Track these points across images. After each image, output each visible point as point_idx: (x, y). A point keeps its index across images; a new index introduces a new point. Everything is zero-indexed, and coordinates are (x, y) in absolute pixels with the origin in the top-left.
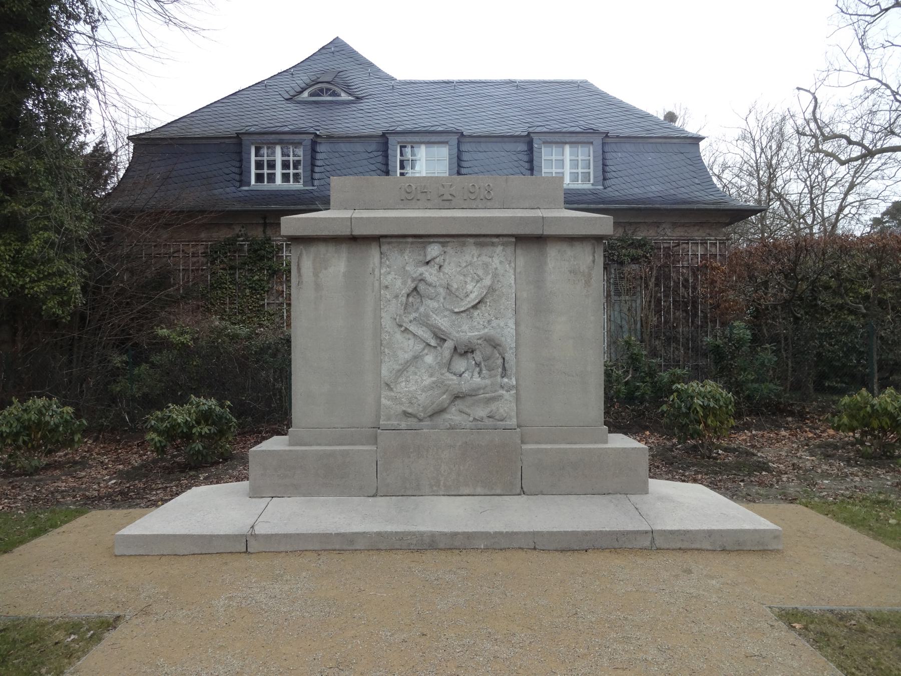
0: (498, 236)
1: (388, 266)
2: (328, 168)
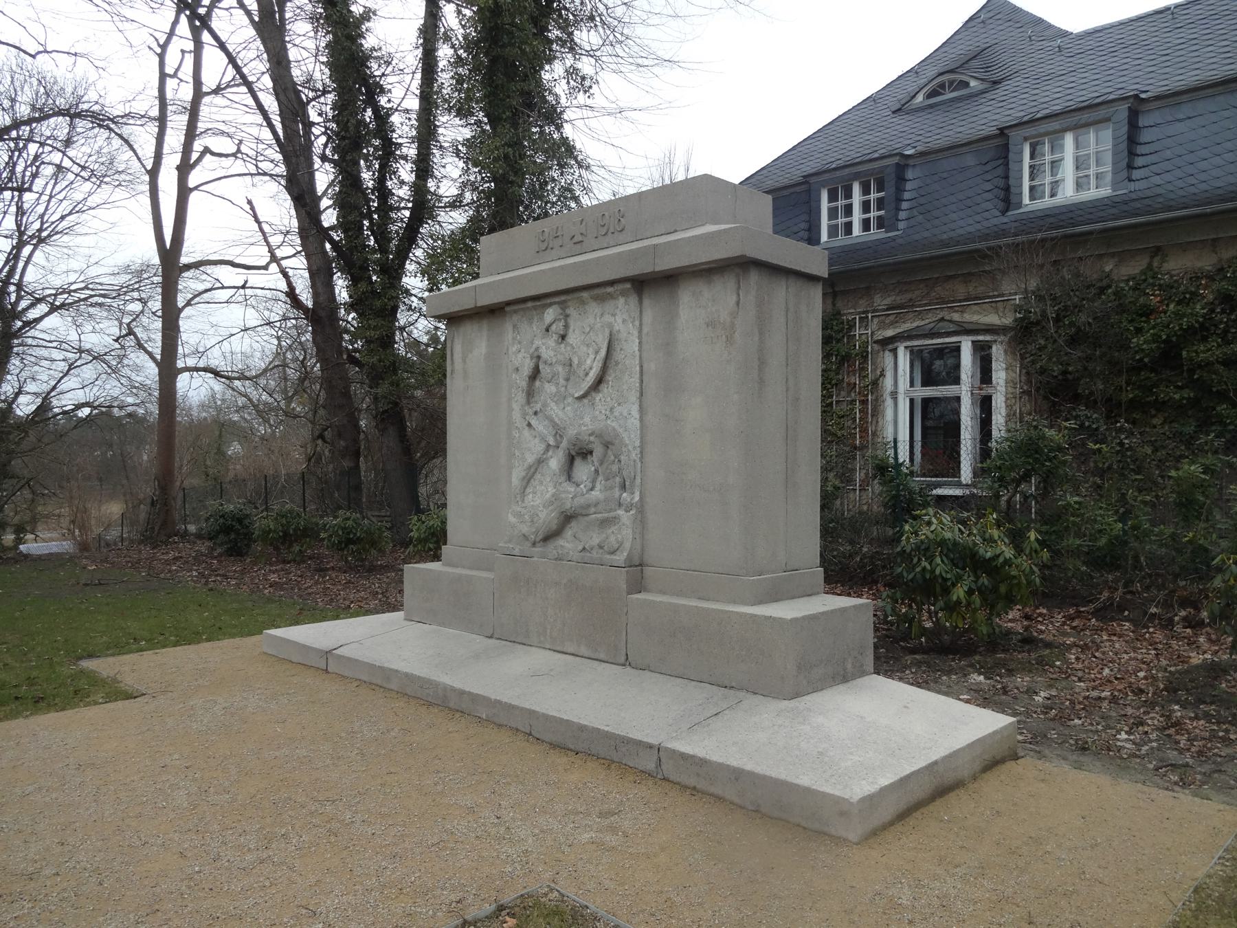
0: (612, 283)
1: (520, 343)
2: (922, 200)
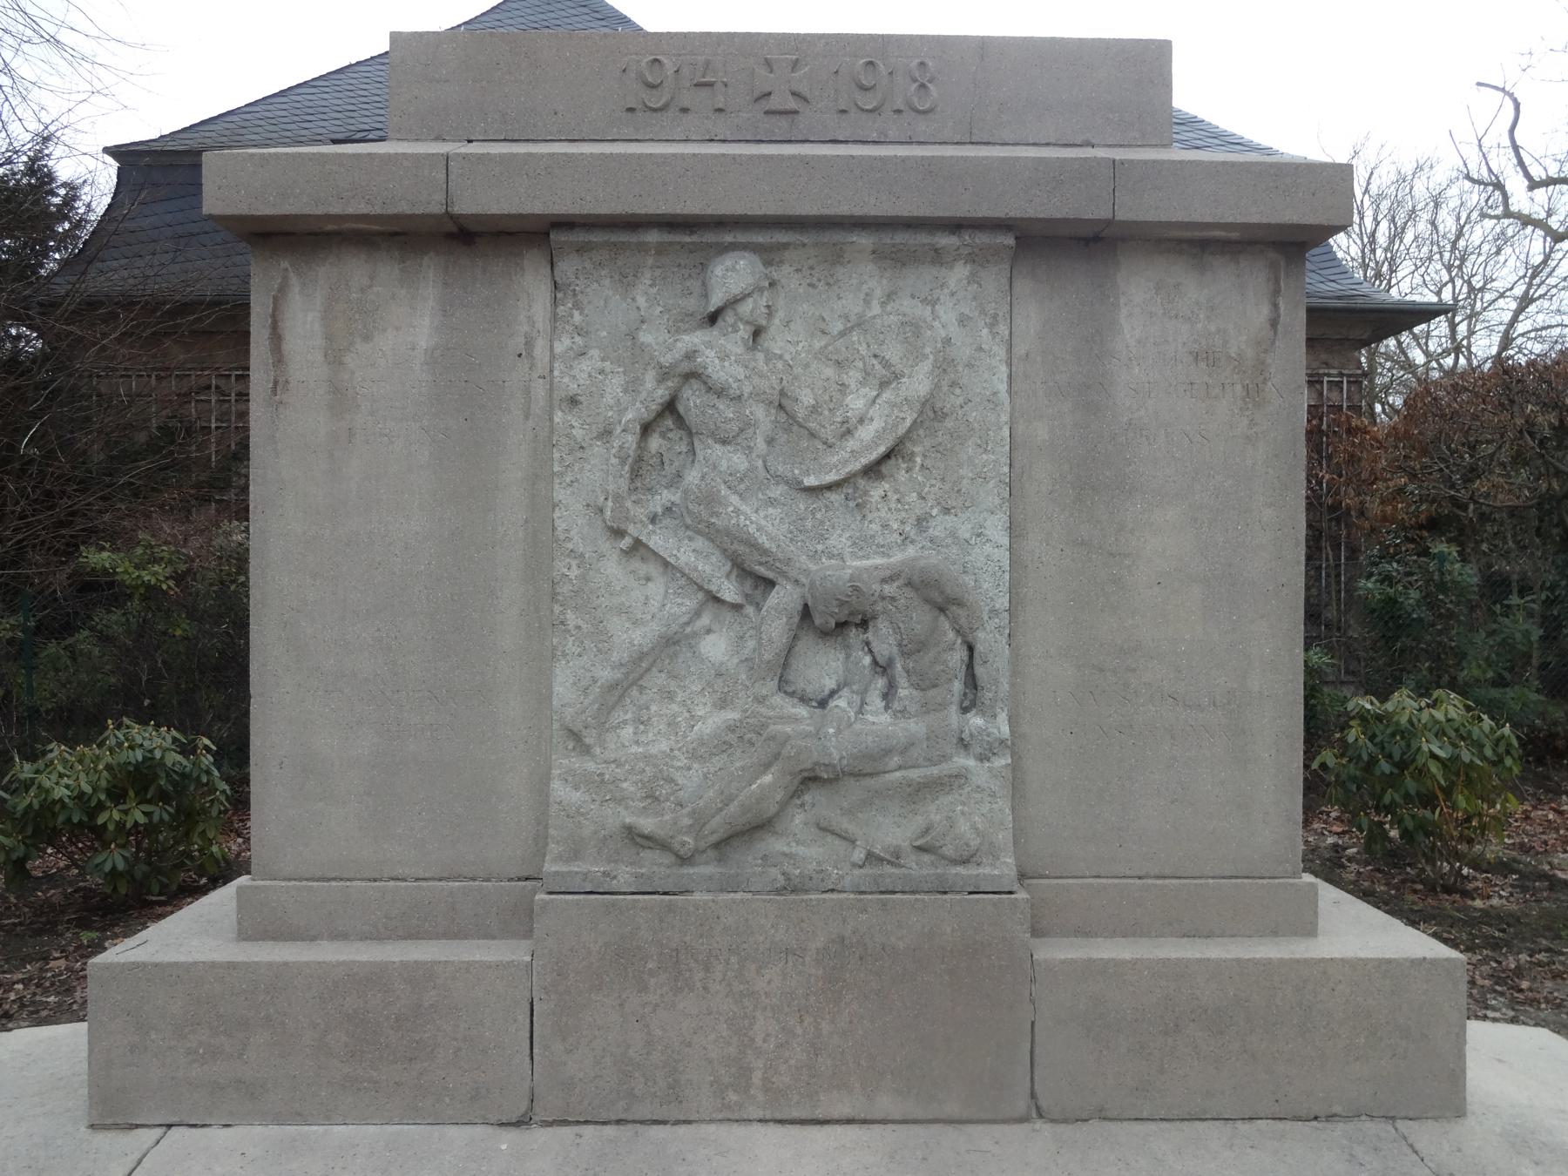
0: (956, 226)
1: (579, 331)
